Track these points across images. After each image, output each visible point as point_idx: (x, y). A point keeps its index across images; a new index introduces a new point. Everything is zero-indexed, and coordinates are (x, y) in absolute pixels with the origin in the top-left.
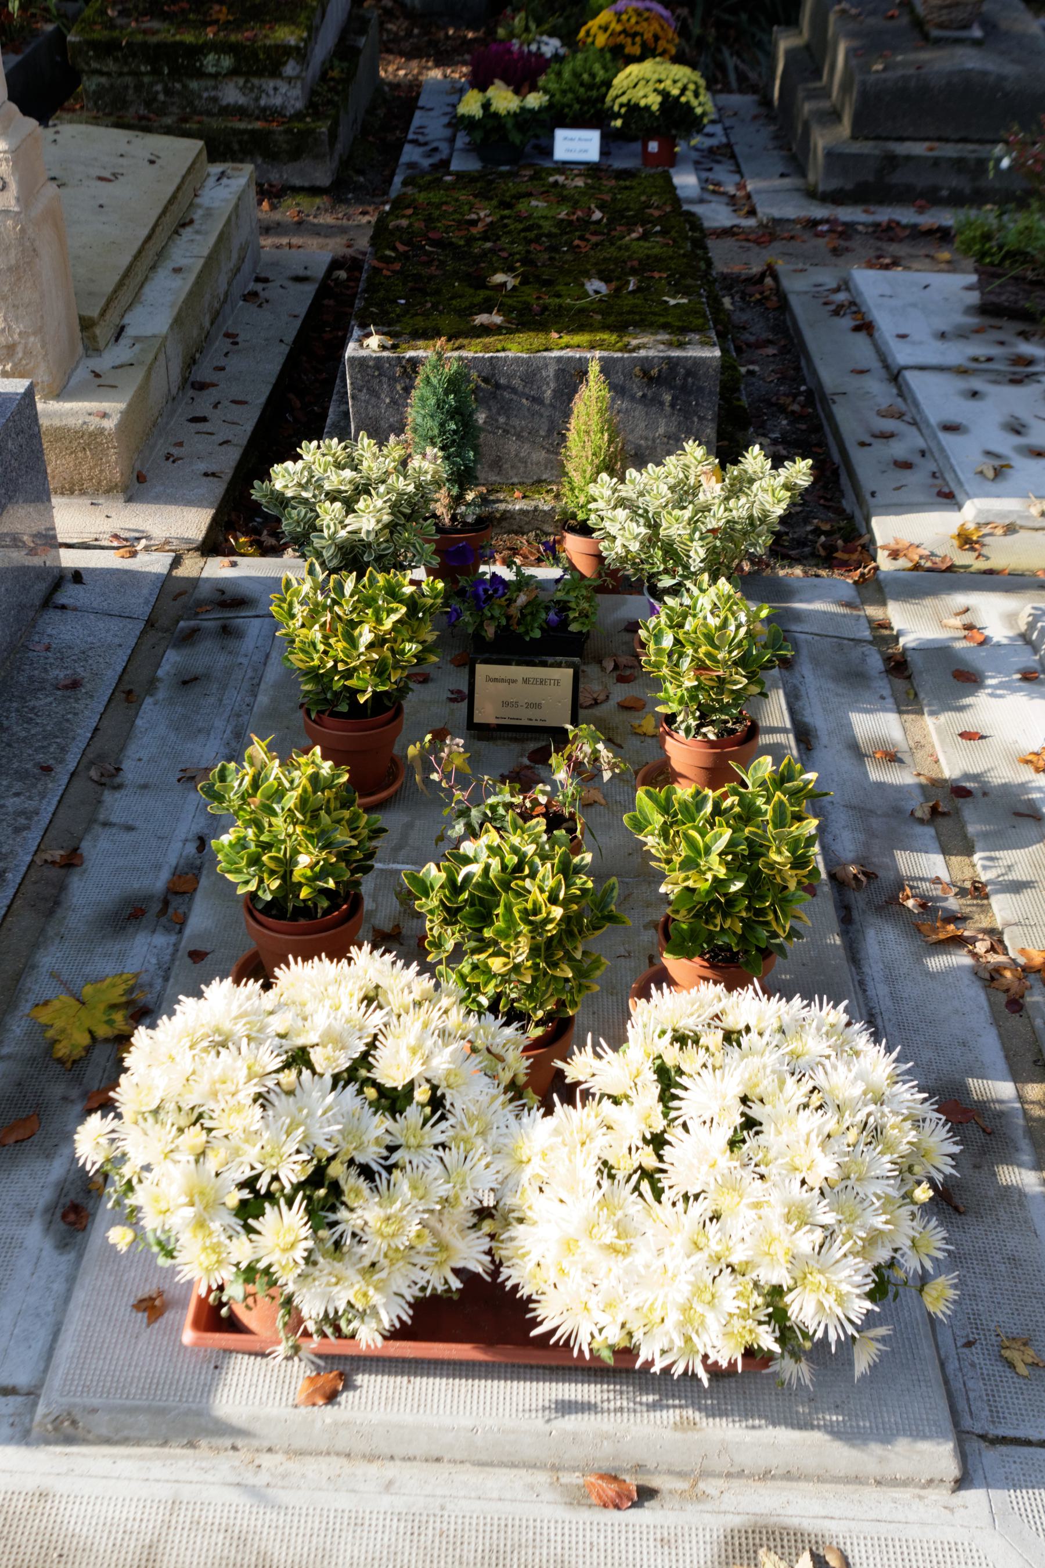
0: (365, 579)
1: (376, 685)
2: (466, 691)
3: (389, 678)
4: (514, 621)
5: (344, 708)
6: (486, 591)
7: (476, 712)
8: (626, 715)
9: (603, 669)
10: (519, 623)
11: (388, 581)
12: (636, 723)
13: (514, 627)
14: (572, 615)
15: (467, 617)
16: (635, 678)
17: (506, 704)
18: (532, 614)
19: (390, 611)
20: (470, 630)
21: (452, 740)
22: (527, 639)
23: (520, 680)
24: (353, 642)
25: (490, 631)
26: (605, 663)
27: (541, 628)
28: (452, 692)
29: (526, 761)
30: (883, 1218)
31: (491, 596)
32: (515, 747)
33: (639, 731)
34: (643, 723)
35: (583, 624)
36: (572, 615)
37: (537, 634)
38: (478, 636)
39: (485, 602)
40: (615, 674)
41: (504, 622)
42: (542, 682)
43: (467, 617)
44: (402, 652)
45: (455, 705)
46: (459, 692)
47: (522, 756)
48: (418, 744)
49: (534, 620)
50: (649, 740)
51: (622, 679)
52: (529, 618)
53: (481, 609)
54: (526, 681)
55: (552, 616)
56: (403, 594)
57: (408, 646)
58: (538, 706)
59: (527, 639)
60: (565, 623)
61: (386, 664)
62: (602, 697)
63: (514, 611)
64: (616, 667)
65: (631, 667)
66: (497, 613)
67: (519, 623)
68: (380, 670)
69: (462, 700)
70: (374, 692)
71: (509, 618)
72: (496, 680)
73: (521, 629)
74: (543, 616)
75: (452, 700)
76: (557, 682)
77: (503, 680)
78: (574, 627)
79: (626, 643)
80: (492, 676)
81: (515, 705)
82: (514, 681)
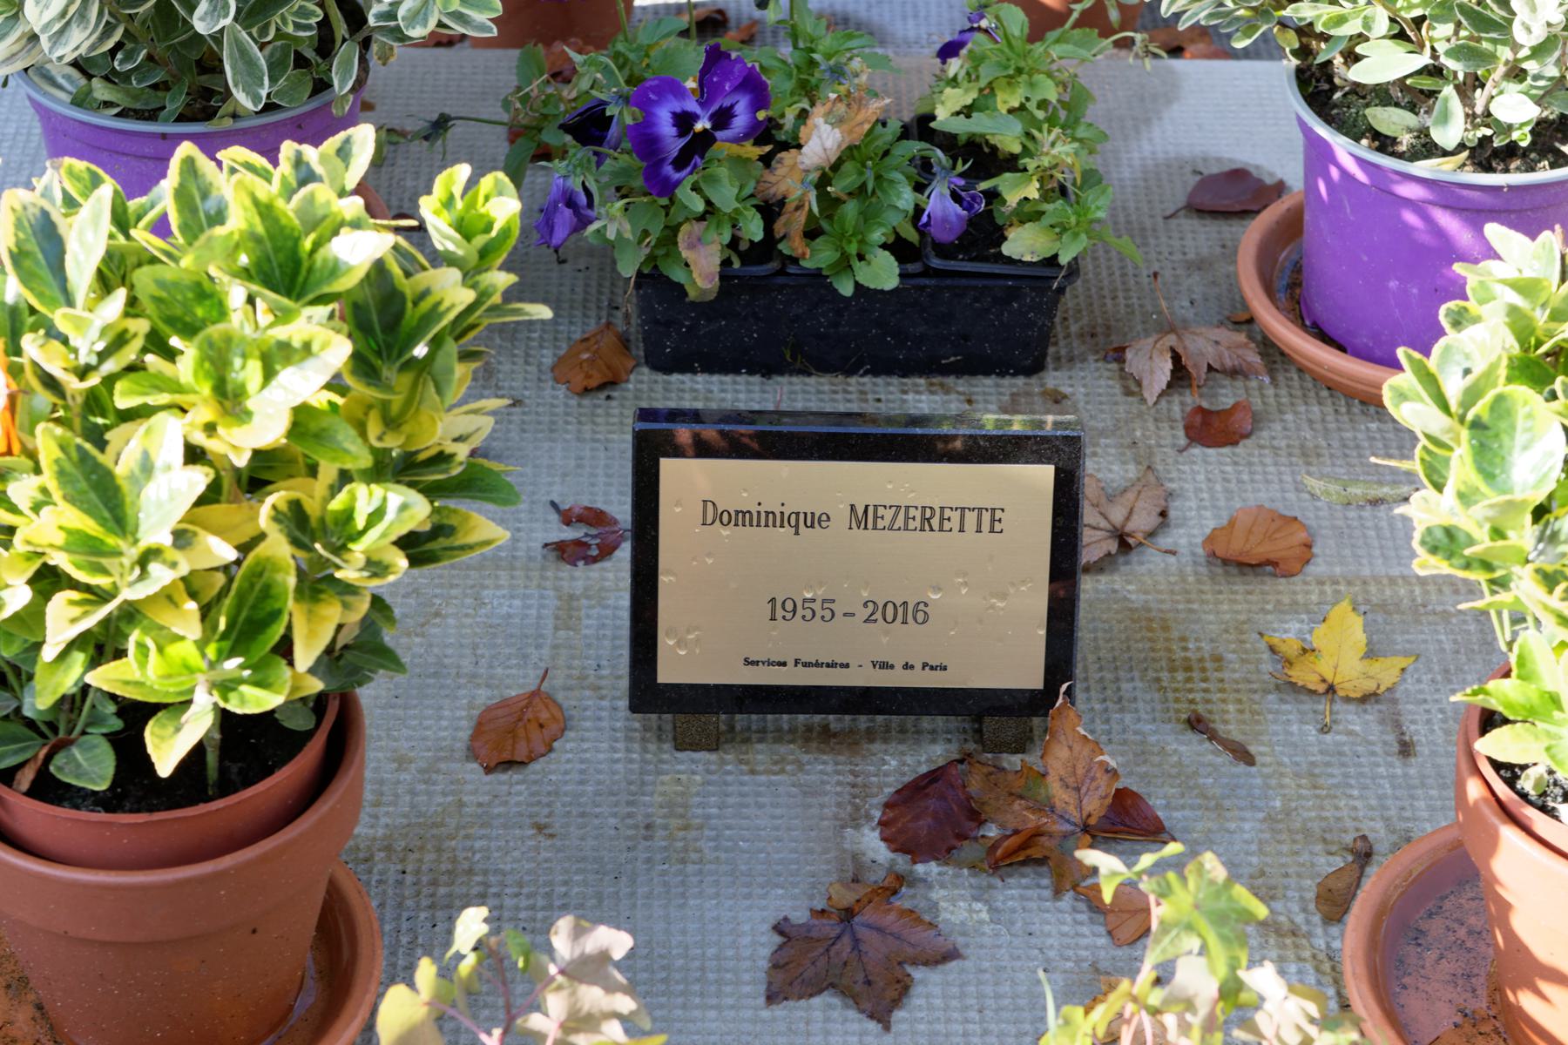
0: (168, 186)
1: (226, 687)
2: (621, 509)
3: (285, 649)
4: (792, 224)
5: (93, 766)
6: (684, 121)
7: (666, 643)
8: (1237, 601)
9: (1132, 386)
10: (812, 233)
11: (265, 211)
12: (1288, 635)
13: (793, 245)
14: (1016, 191)
15: (613, 221)
16: (1258, 421)
17: (782, 609)
18: (860, 192)
19: (274, 359)
20: (628, 268)
21: (578, 933)
22: (846, 289)
23: (841, 515)
24: (105, 497)
25: (701, 267)
26: (1135, 361)
27: (898, 248)
28: (567, 518)
29: (872, 845)
30: (960, 162)
31: (706, 139)
32: (825, 773)
33: (1303, 675)
34: (1320, 637)
35: (1060, 229)
36: (1016, 191)
37: (883, 273)
38: (656, 283)
39: (681, 162)
40: (1181, 405)
41: (754, 229)
42: (929, 519)
43: (613, 221)
44: (341, 532)
45: (581, 576)
46: (594, 517)
47: (856, 820)
48: (426, 971)
49: (868, 217)
50: (1354, 720)
51: (1210, 429)
52: (851, 209)
53: (667, 188)
54: (863, 518)
55: (939, 202)
56: (335, 269)
57: (364, 498)
58: (912, 612)
59: (846, 289)
60: (985, 231)
61: (267, 592)
62: (1142, 522)
63: (791, 179)
64: (1180, 375)
65: (1234, 373)
66: (726, 195)
67: (812, 233)
68: (245, 618)
69: (606, 551)
70: (226, 719)
71: (770, 210)
72: (741, 517)
73: (819, 257)
74: (906, 198)
75: (566, 552)
76: (992, 519)
77: (771, 519)
78: (1023, 244)
79: (1200, 265)
80: (728, 504)
81: (826, 610)
82: (814, 521)
